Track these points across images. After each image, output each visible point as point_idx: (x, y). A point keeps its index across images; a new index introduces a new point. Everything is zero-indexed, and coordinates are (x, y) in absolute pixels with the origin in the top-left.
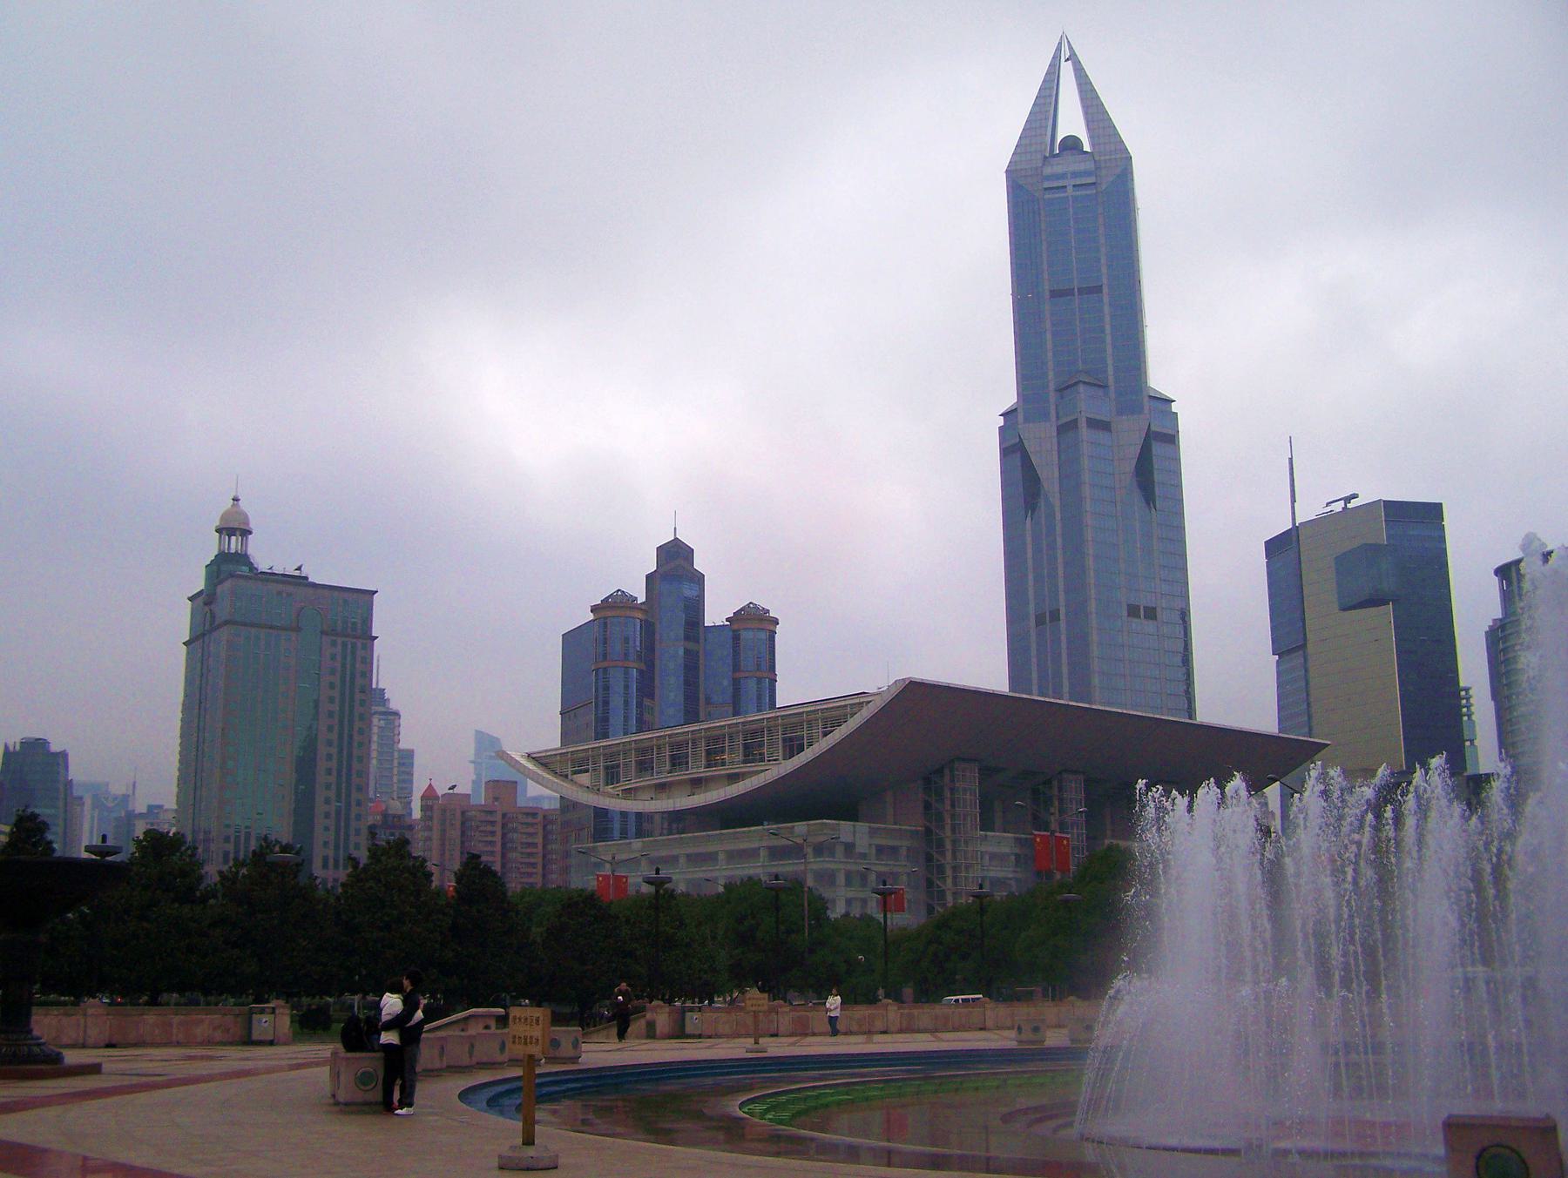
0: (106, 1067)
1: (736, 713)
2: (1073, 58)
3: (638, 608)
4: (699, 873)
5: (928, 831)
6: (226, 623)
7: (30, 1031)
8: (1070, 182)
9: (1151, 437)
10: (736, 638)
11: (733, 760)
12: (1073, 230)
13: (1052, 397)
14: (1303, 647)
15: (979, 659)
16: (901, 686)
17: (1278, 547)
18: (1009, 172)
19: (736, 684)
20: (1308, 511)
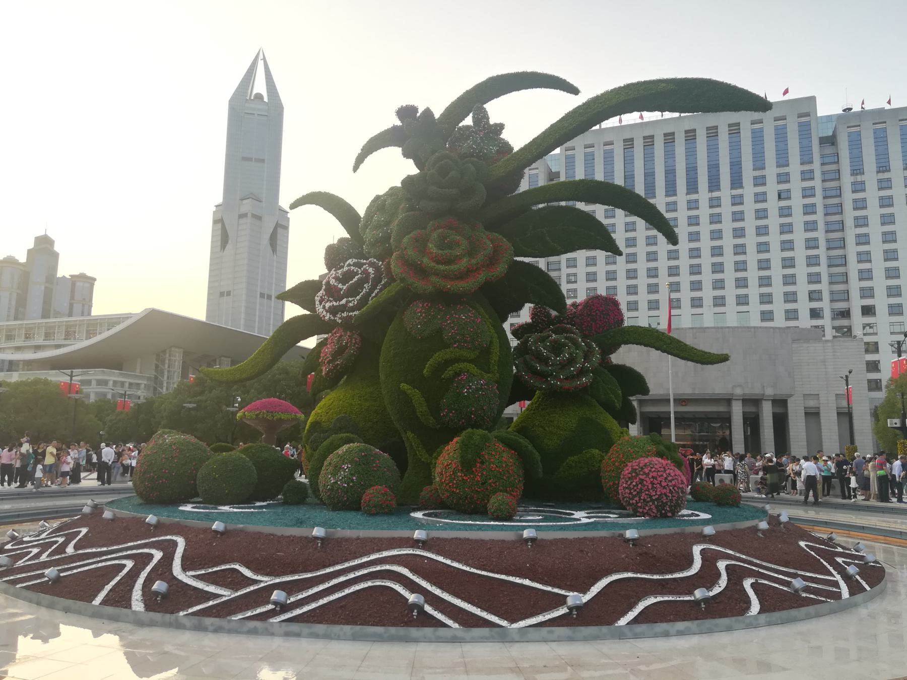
2: (264, 59)
5: (156, 378)
9: (278, 226)
11: (59, 339)
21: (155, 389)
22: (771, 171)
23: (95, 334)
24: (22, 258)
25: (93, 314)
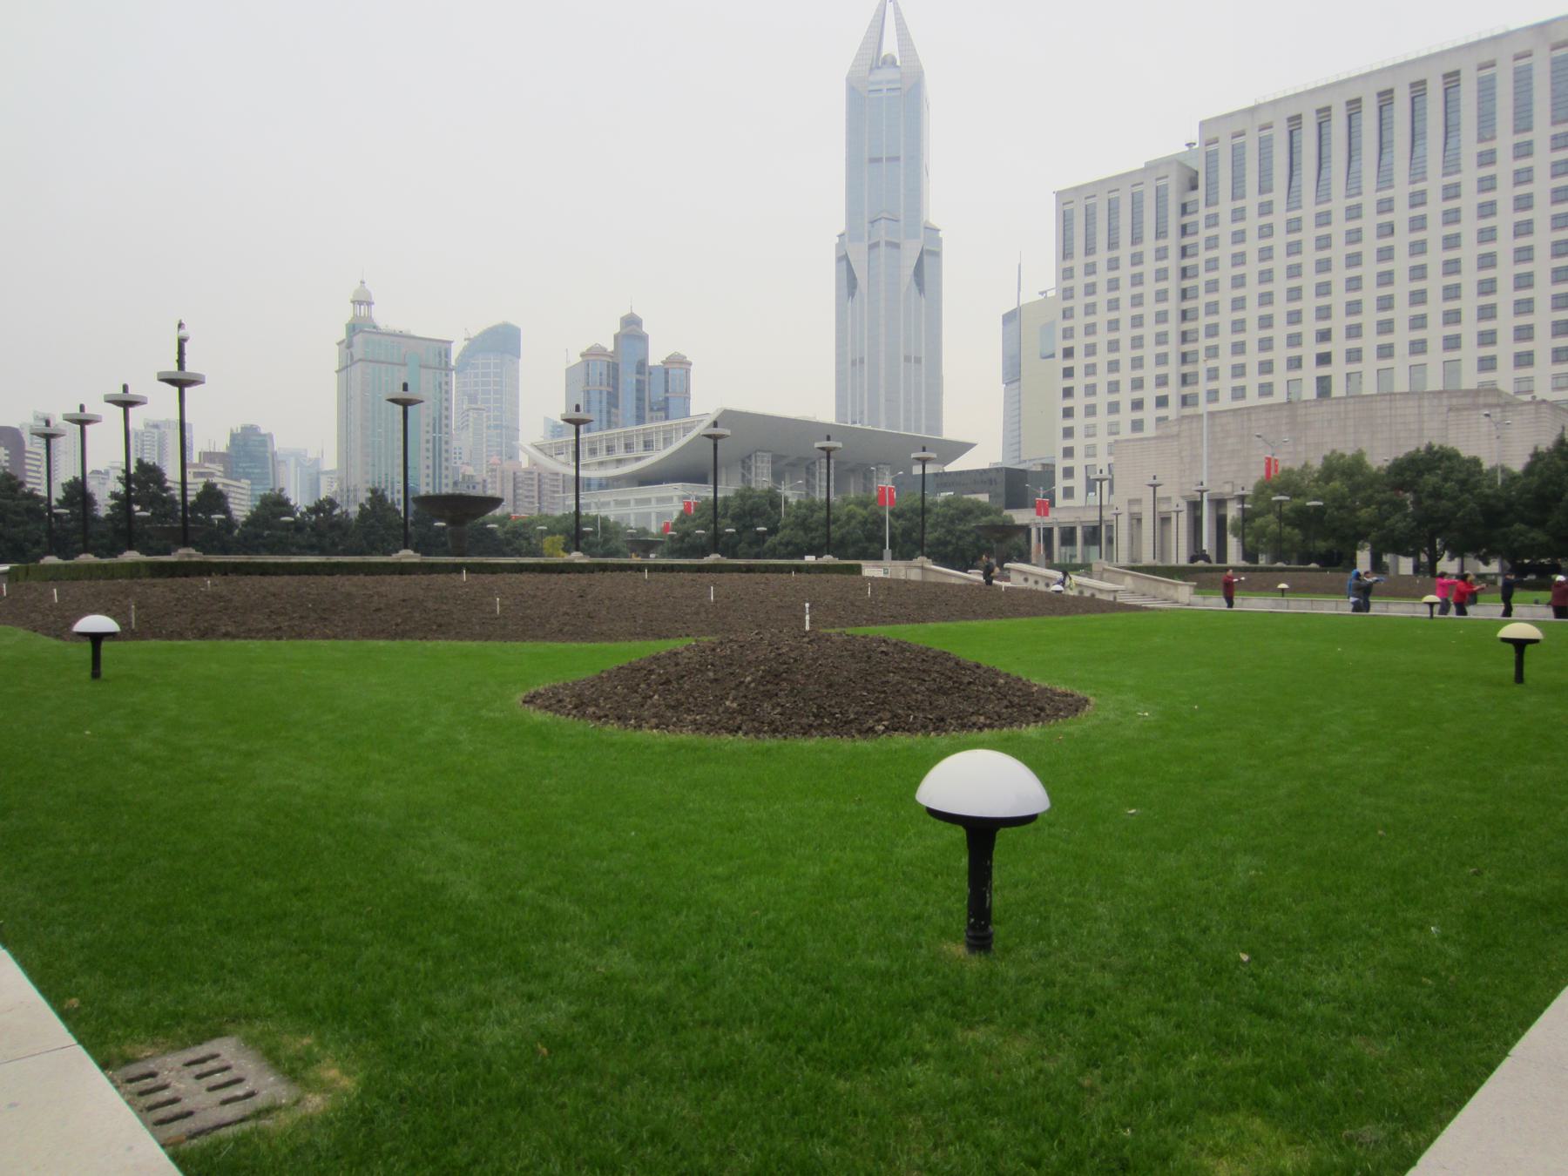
4: (622, 511)
10: (667, 372)
11: (639, 451)
17: (1010, 318)
22: (1505, 140)
24: (610, 347)
25: (692, 413)
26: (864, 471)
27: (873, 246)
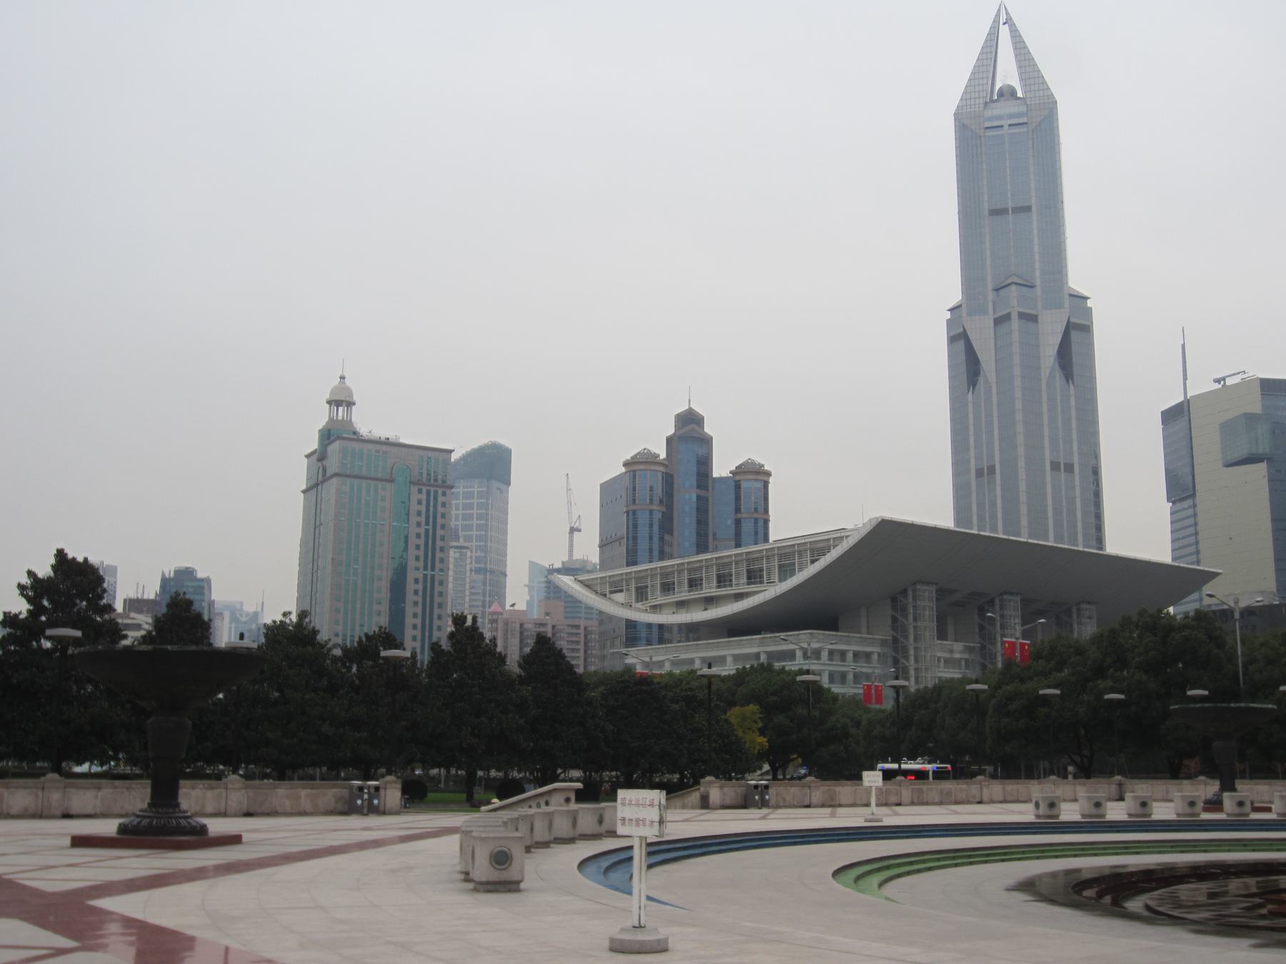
0: (245, 837)
1: (738, 545)
2: (1009, 21)
3: (660, 463)
5: (895, 640)
6: (336, 475)
7: (178, 805)
8: (1005, 123)
9: (1069, 328)
10: (738, 486)
11: (740, 585)
12: (1008, 157)
13: (991, 295)
14: (1193, 495)
15: (930, 502)
16: (874, 523)
17: (1176, 416)
18: (957, 116)
19: (738, 522)
20: (1201, 385)
21: (984, 667)
23: (793, 573)
25: (771, 539)
26: (1061, 613)
27: (1000, 321)
